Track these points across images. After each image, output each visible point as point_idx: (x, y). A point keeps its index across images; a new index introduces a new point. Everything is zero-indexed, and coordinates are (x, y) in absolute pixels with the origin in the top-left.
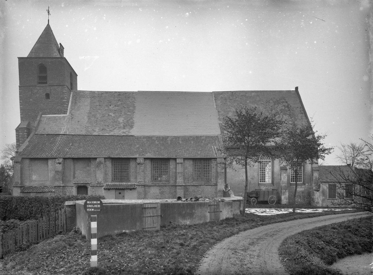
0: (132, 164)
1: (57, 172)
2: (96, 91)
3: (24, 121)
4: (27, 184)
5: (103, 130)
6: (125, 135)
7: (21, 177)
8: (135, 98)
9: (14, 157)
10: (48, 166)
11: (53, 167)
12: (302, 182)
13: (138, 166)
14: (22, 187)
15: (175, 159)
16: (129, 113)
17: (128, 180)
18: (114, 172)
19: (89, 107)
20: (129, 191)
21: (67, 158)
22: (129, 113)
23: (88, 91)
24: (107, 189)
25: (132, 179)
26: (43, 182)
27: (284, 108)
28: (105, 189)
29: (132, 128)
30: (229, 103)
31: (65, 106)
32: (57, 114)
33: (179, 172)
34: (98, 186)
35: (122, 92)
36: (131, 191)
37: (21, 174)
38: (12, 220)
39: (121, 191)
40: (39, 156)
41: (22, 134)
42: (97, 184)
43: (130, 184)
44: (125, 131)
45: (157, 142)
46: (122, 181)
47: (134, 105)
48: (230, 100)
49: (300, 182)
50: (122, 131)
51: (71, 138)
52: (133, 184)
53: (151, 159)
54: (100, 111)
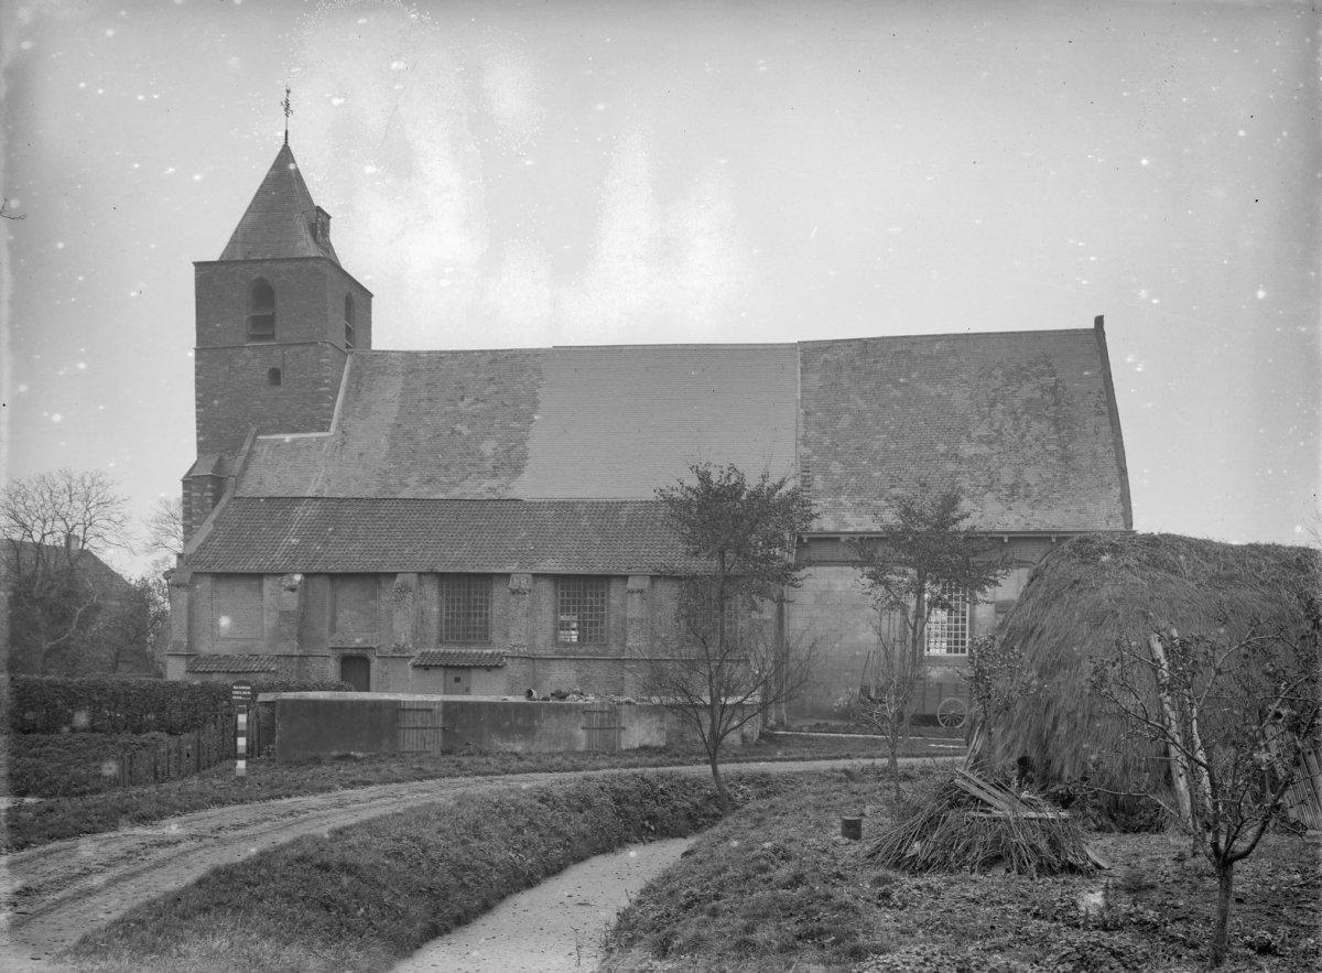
0: (499, 592)
1: (284, 614)
2: (424, 352)
3: (205, 455)
4: (205, 648)
5: (429, 481)
6: (494, 497)
7: (190, 628)
8: (539, 371)
9: (172, 571)
10: (262, 596)
11: (277, 598)
12: (967, 654)
13: (513, 599)
14: (191, 657)
15: (625, 578)
16: (515, 424)
17: (485, 639)
18: (447, 615)
19: (395, 408)
20: (484, 675)
21: (316, 574)
22: (515, 424)
23: (398, 352)
24: (420, 666)
25: (496, 636)
26: (249, 643)
27: (1038, 394)
28: (415, 666)
29: (520, 473)
30: (846, 383)
31: (325, 405)
32: (303, 432)
33: (633, 619)
34: (394, 657)
35: (502, 351)
36: (489, 675)
37: (190, 620)
38: (153, 734)
39: (459, 674)
40: (238, 568)
41: (198, 494)
42: (394, 651)
43: (490, 651)
44: (494, 483)
45: (584, 522)
46: (466, 644)
47: (535, 394)
48: (854, 369)
49: (960, 655)
50: (487, 483)
51: (333, 508)
52: (498, 654)
53: (556, 578)
54: (427, 420)
